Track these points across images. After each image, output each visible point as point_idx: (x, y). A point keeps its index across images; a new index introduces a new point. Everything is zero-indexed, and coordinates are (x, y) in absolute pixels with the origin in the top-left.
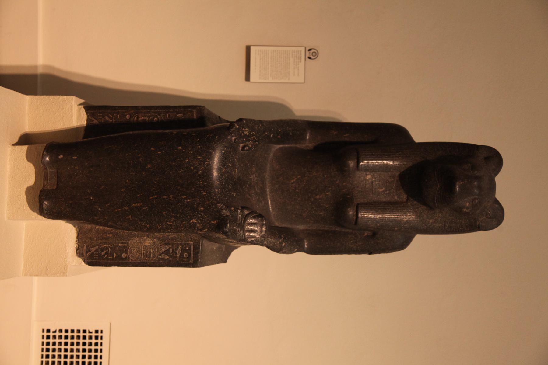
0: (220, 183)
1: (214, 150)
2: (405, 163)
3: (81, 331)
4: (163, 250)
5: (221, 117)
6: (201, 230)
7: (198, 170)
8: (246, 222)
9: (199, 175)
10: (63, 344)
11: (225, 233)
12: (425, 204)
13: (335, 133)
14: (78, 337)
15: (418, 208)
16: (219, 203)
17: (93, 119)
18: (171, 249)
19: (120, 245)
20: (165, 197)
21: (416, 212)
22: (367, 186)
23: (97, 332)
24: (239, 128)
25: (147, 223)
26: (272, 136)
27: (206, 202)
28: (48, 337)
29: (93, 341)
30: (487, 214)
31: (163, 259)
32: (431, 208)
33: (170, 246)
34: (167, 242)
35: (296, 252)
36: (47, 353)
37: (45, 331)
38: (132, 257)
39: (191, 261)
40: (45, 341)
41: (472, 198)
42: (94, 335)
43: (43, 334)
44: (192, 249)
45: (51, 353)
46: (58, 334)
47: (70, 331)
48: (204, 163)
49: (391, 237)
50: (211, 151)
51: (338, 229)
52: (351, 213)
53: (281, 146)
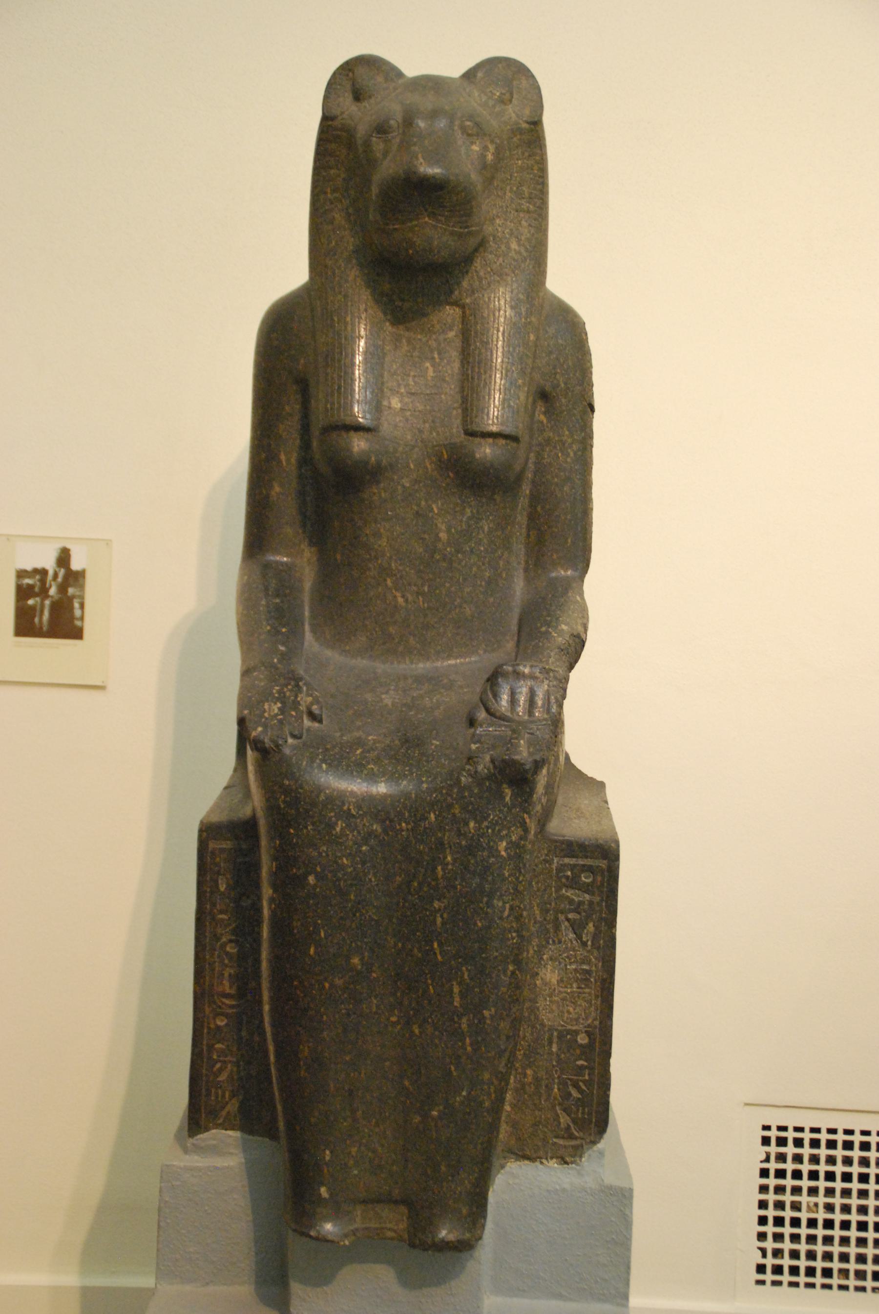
0: (405, 776)
1: (320, 789)
2: (362, 307)
3: (764, 1181)
4: (572, 936)
5: (225, 784)
6: (526, 830)
7: (371, 834)
8: (509, 714)
9: (385, 831)
10: (795, 1231)
11: (538, 765)
12: (468, 260)
13: (277, 489)
14: (780, 1190)
15: (480, 279)
16: (458, 781)
17: (224, 1113)
18: (570, 916)
19: (554, 1049)
20: (439, 920)
21: (489, 284)
22: (421, 408)
23: (766, 1141)
24: (265, 726)
25: (505, 971)
26: (282, 648)
27: (454, 815)
28: (778, 1270)
29: (790, 1150)
30: (502, 101)
31: (595, 937)
32: (482, 244)
33: (561, 917)
34: (550, 926)
35: (583, 599)
36: (819, 1272)
37: (761, 1277)
38: (587, 1018)
39: (603, 864)
40: (786, 1278)
41: (459, 134)
42: (773, 1149)
43: (768, 1283)
44: (573, 861)
45: (819, 1264)
46: (770, 1245)
47: (763, 1213)
48: (354, 816)
49: (551, 352)
50: (322, 797)
51: (526, 489)
52: (488, 451)
53: (307, 627)
